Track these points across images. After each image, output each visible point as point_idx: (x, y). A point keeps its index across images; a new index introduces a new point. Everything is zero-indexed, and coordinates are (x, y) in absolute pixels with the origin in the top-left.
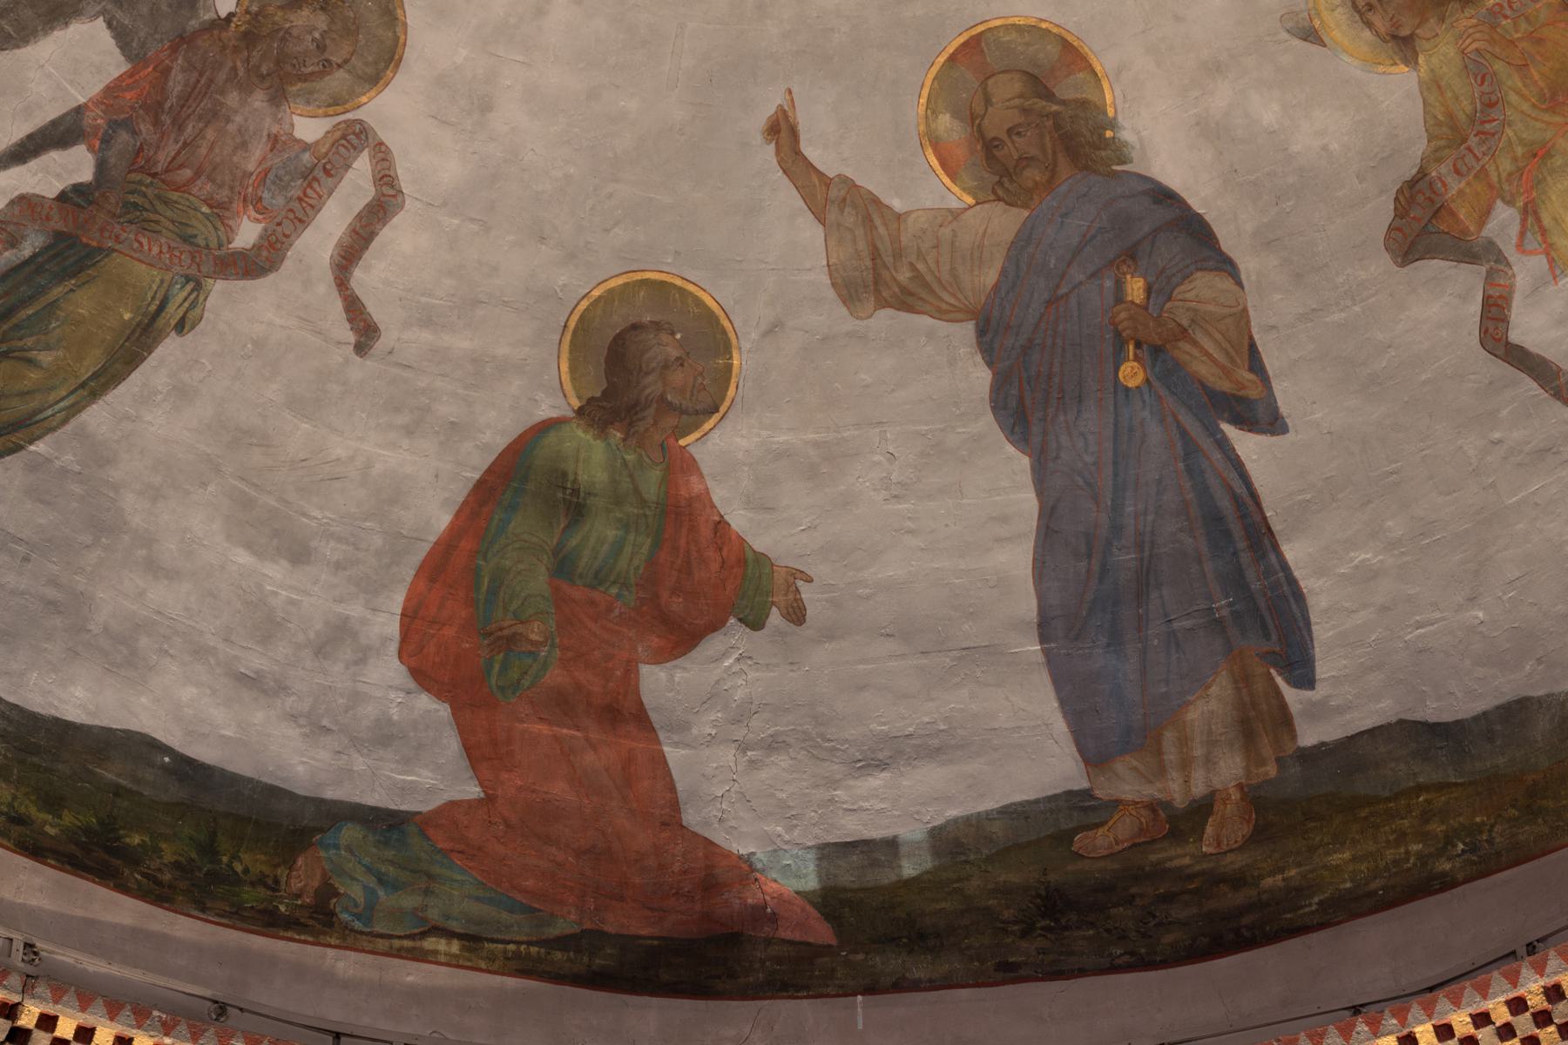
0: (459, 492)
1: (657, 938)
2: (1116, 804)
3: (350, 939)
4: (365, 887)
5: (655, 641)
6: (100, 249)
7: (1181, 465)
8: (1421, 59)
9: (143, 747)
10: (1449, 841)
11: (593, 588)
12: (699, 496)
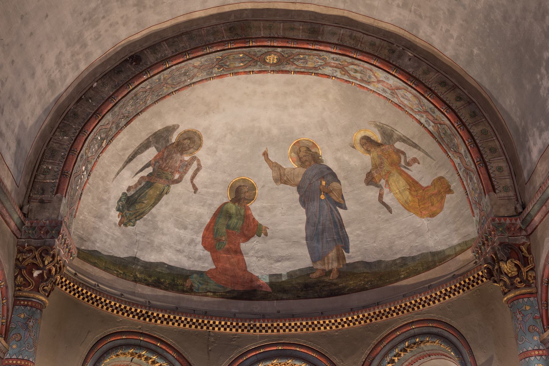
0: (211, 215)
1: (244, 290)
2: (317, 269)
3: (195, 294)
4: (198, 285)
5: (243, 239)
6: (154, 183)
7: (330, 213)
8: (371, 154)
9: (162, 264)
10: (368, 282)
11: (233, 230)
12: (250, 214)
